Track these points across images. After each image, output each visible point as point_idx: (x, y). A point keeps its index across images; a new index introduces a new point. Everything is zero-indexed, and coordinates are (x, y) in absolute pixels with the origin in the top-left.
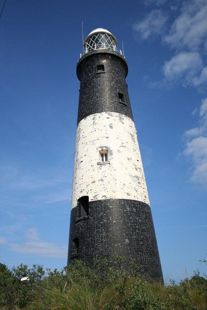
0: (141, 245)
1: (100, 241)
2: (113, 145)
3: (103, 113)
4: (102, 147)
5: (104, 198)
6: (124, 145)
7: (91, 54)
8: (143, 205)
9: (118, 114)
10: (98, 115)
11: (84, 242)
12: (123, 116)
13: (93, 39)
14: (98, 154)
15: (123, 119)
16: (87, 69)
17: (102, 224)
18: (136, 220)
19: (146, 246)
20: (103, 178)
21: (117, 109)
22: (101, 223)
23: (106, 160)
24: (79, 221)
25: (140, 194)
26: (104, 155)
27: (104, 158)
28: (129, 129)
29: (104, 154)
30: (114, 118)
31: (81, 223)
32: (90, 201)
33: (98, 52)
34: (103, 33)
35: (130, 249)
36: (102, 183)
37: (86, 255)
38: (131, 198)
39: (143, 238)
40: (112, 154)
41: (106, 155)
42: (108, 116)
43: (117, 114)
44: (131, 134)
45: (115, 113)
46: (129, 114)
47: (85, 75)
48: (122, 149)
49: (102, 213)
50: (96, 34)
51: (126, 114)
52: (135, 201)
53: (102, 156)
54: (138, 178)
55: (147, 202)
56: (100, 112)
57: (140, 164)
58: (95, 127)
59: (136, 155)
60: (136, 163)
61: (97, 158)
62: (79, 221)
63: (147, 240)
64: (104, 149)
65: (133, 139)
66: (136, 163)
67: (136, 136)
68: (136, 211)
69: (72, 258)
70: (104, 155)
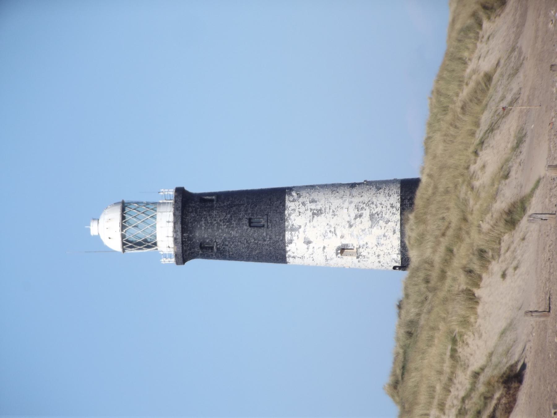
9: (286, 233)
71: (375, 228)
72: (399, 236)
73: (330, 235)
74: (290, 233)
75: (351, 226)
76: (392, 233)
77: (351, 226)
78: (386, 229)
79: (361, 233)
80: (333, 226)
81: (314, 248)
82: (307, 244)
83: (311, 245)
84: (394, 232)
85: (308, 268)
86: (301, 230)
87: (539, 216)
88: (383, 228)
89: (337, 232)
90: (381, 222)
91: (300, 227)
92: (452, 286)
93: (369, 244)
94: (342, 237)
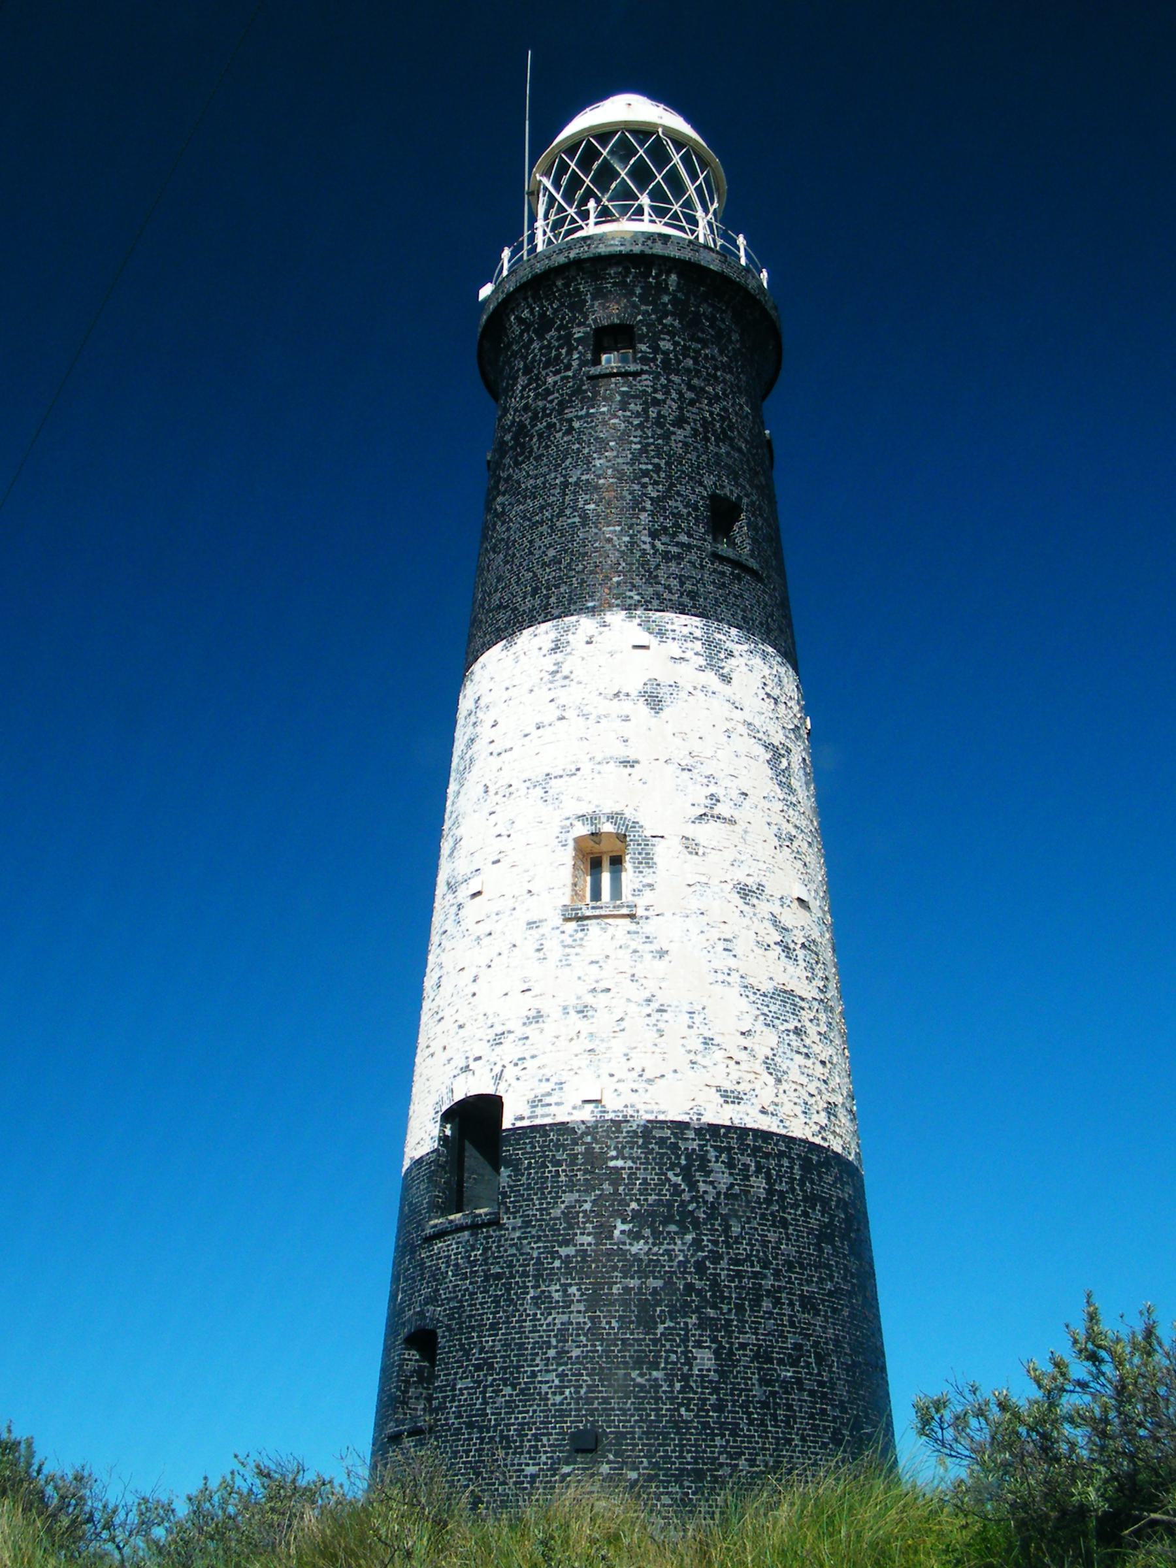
0: (785, 1383)
1: (552, 1353)
2: (657, 808)
3: (609, 617)
4: (593, 819)
5: (586, 1114)
6: (723, 809)
7: (562, 259)
8: (813, 1160)
9: (696, 621)
10: (585, 625)
11: (467, 1354)
12: (730, 637)
13: (585, 164)
14: (567, 855)
15: (731, 654)
16: (536, 345)
17: (567, 1260)
18: (765, 1243)
19: (812, 1393)
20: (589, 999)
21: (693, 595)
22: (564, 1251)
23: (616, 892)
24: (440, 1235)
25: (792, 1094)
26: (606, 863)
27: (606, 877)
28: (757, 709)
29: (602, 856)
30: (674, 648)
31: (450, 1247)
32: (506, 1124)
33: (603, 250)
34: (643, 132)
35: (719, 1407)
36: (584, 1026)
37: (470, 1425)
38: (749, 1116)
39: (797, 1347)
40: (647, 861)
41: (617, 862)
42: (644, 638)
43: (691, 624)
44: (1149, 1333)
45: (684, 619)
46: (777, 629)
47: (522, 381)
48: (706, 833)
49: (569, 1198)
50: (603, 134)
51: (748, 626)
52: (766, 1136)
53: (595, 866)
54: (786, 996)
55: (840, 1141)
56: (592, 611)
57: (810, 925)
58: (563, 696)
59: (794, 878)
60: (793, 917)
61: (558, 873)
62: (440, 1235)
63: (820, 1359)
64: (608, 828)
65: (782, 777)
66: (793, 917)
67: (798, 753)
68: (770, 1191)
69: (387, 1441)
70: (606, 863)
71: (744, 1004)
72: (710, 1118)
73: (700, 794)
74: (698, 633)
75: (745, 892)
76: (728, 1085)
77: (745, 892)
78: (742, 1056)
79: (714, 934)
80: (737, 815)
81: (627, 719)
82: (643, 694)
83: (643, 709)
84: (731, 1097)
85: (855, 1073)
86: (711, 678)
87: (603, 912)
88: (744, 1042)
89: (712, 826)
90: (772, 1038)
91: (726, 679)
92: (555, 649)
93: (660, 966)
94: (691, 846)
